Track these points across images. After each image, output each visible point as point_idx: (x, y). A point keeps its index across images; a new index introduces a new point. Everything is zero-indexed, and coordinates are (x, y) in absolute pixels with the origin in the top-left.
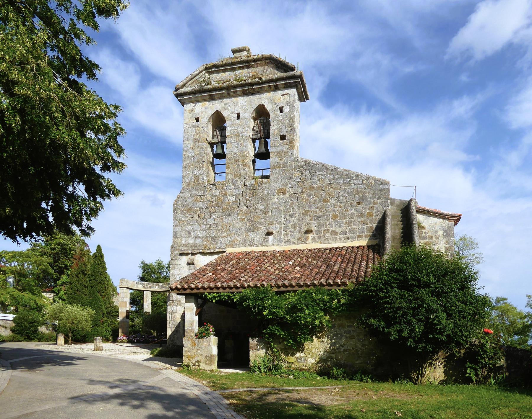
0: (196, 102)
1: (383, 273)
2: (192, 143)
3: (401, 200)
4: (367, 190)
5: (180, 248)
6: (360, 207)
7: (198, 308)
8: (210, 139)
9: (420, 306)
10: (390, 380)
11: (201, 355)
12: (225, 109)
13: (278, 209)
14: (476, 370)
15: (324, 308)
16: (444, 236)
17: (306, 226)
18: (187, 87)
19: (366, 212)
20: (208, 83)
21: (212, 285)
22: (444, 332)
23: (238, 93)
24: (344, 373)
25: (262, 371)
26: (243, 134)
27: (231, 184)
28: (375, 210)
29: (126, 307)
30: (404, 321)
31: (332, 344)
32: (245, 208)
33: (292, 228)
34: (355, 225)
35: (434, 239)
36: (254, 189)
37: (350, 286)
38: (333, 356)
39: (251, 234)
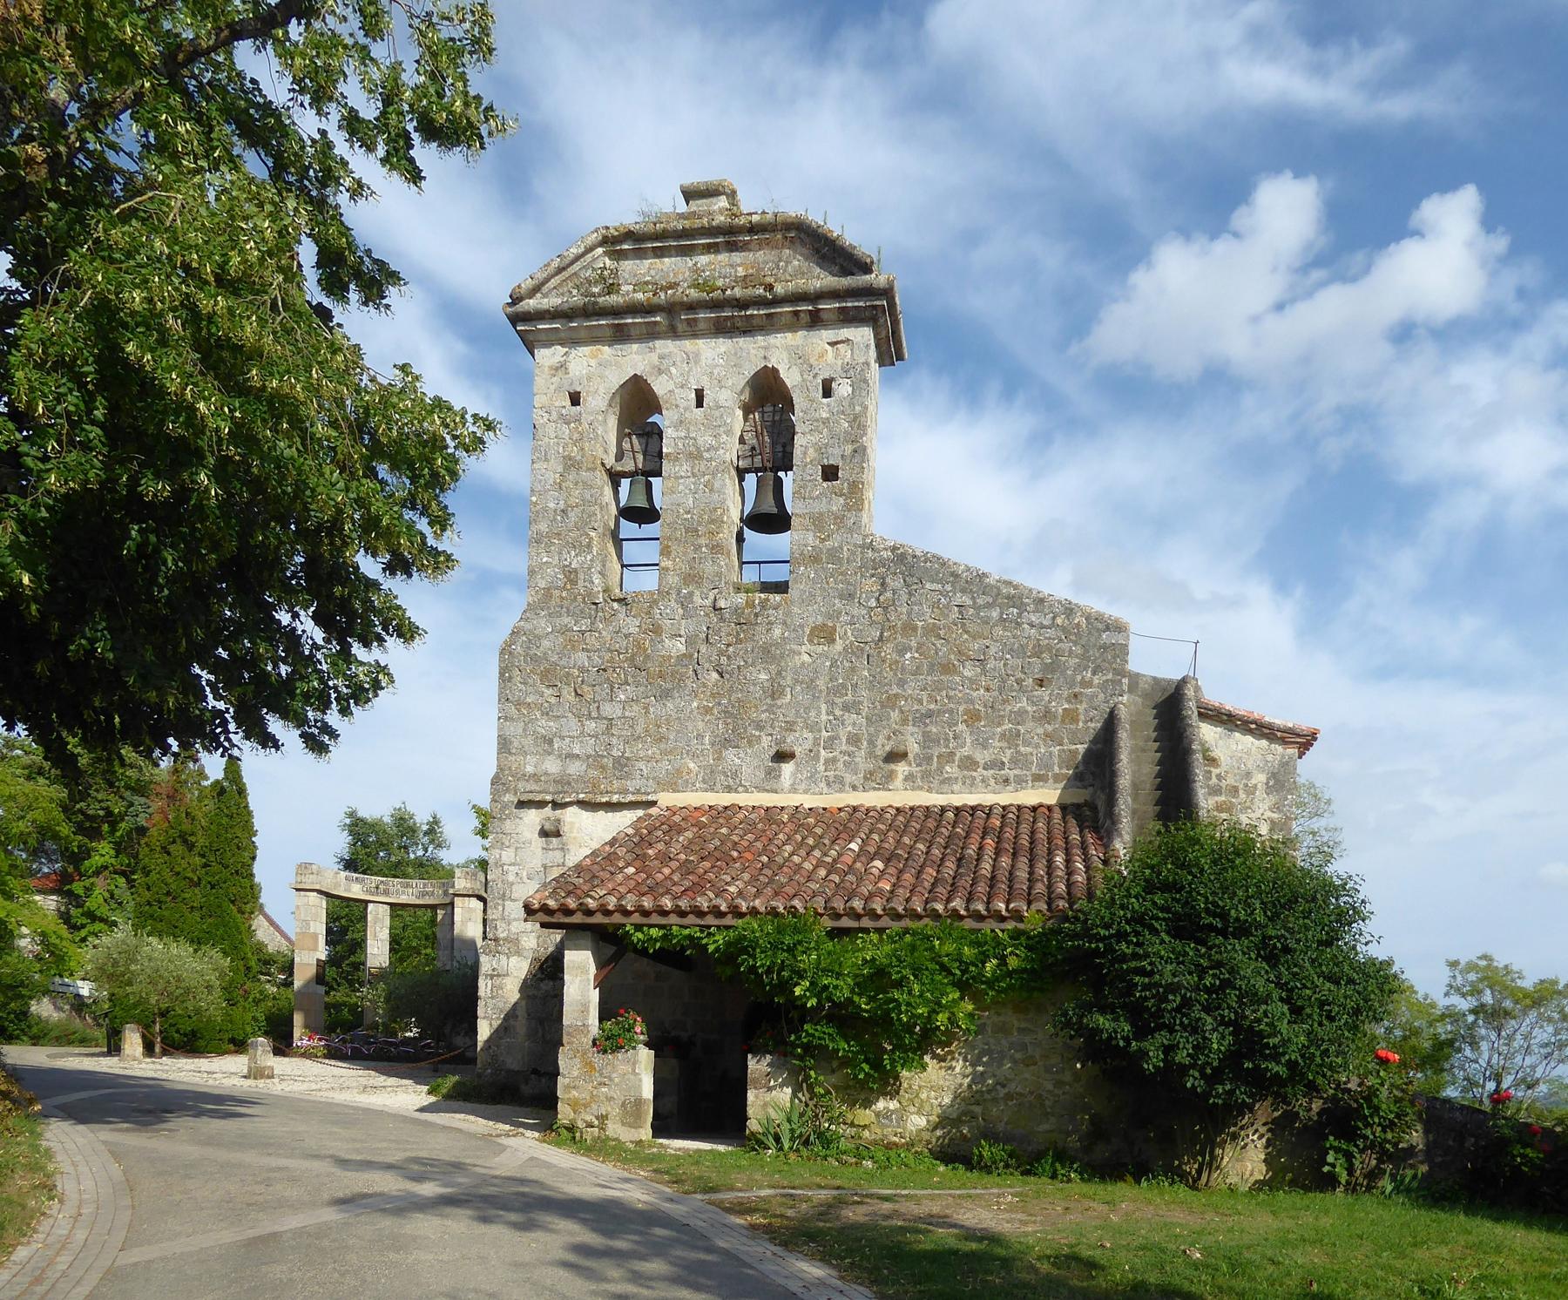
0: (573, 342)
1: (1128, 890)
2: (560, 469)
3: (1155, 678)
4: (1066, 646)
5: (520, 785)
6: (1044, 694)
7: (600, 965)
8: (610, 461)
9: (1226, 984)
10: (1129, 1178)
11: (610, 1099)
12: (660, 372)
13: (810, 685)
14: (1349, 1156)
15: (960, 980)
16: (1269, 790)
17: (889, 738)
18: (545, 296)
19: (1060, 707)
20: (611, 289)
21: (647, 903)
22: (1284, 1054)
23: (702, 325)
24: (1010, 1156)
25: (786, 1146)
26: (712, 453)
27: (673, 603)
28: (1084, 705)
29: (315, 949)
30: (1182, 1023)
31: (978, 1078)
32: (715, 675)
33: (848, 742)
34: (1027, 743)
35: (1242, 796)
36: (744, 622)
37: (1034, 918)
38: (977, 1109)
39: (730, 754)
